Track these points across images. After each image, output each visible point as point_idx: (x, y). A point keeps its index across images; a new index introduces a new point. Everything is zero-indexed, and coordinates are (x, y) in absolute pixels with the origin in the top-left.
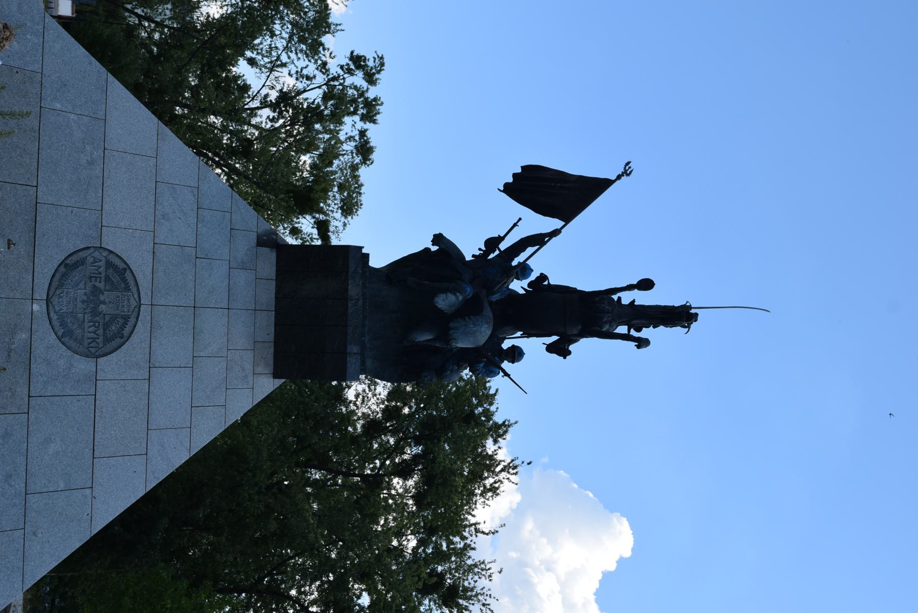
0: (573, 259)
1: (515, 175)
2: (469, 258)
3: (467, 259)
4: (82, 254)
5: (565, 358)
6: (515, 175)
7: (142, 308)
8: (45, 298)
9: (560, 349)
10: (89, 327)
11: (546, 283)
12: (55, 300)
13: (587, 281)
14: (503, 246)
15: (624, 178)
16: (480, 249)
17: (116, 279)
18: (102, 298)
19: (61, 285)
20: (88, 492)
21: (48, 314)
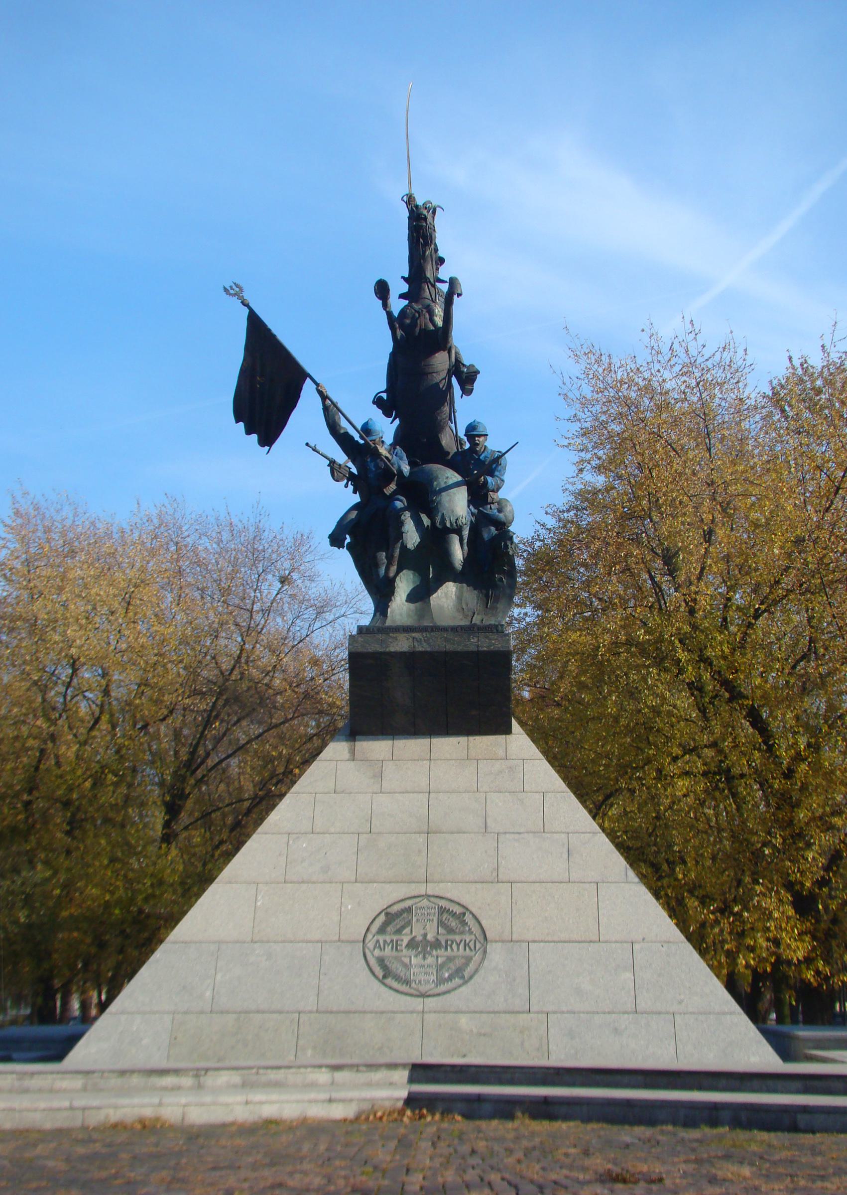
0: (349, 367)
1: (248, 432)
2: (357, 498)
3: (359, 500)
4: (373, 962)
5: (479, 372)
6: (248, 432)
7: (430, 892)
8: (421, 1000)
9: (467, 378)
10: (452, 950)
11: (384, 396)
12: (423, 988)
13: (382, 344)
14: (341, 457)
15: (246, 296)
16: (346, 486)
17: (399, 923)
18: (419, 938)
19: (407, 982)
20: (636, 946)
21: (438, 995)
